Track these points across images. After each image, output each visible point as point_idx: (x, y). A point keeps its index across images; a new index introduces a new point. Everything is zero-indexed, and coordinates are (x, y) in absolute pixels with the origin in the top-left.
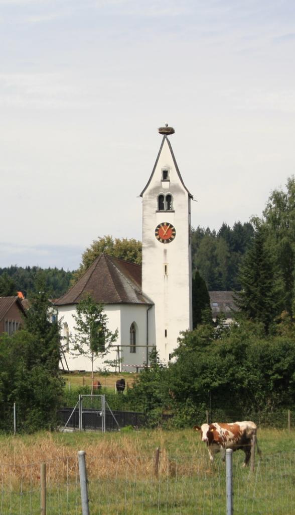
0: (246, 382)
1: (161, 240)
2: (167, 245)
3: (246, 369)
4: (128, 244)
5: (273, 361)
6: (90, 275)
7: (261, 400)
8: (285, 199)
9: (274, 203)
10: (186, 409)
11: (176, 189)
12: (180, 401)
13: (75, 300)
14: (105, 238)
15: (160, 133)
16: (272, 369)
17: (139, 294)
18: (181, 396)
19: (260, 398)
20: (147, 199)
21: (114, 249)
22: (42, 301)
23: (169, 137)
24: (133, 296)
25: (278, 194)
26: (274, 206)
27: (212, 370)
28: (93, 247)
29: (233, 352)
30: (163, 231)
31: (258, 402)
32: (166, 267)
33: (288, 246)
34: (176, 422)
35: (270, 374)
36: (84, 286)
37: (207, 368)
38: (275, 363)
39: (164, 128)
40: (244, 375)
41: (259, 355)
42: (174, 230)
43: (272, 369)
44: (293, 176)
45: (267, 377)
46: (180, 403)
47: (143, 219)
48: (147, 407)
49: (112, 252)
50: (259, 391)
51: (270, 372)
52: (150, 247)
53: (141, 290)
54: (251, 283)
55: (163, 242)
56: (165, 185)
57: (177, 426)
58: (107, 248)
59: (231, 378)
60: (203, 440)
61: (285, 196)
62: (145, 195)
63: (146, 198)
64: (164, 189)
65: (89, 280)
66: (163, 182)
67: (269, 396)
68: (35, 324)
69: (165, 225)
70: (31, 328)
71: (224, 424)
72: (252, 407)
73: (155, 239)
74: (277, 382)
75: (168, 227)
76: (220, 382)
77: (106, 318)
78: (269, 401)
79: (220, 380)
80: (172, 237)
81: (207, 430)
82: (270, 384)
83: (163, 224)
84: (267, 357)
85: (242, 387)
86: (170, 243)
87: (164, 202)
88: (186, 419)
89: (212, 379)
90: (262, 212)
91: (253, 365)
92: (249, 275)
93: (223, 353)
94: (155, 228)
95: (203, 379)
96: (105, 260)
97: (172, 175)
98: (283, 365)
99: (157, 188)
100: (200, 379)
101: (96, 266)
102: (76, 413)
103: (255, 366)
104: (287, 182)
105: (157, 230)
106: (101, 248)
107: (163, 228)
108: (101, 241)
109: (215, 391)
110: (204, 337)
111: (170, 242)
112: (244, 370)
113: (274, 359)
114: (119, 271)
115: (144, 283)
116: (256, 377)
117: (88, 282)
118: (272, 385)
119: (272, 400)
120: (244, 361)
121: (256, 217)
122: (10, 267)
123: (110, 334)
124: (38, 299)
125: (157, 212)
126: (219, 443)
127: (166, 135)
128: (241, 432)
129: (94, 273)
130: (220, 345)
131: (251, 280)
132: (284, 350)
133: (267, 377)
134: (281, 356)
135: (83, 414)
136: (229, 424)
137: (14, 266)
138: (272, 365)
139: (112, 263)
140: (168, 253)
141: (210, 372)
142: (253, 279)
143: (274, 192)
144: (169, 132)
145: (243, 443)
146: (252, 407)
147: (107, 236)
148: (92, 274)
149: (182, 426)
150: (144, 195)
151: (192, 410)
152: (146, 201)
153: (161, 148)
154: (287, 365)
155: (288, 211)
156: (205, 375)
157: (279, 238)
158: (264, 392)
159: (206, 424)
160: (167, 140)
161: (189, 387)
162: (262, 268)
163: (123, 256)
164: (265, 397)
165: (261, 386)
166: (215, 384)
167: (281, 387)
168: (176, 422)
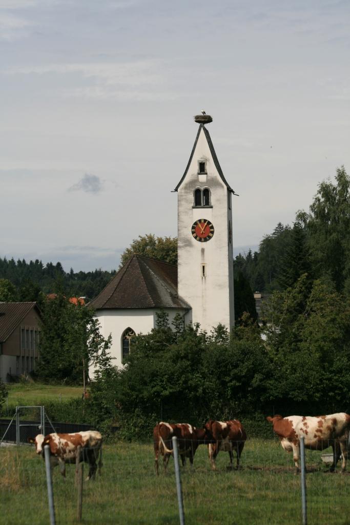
0: (200, 390)
1: (198, 238)
2: (204, 243)
3: (201, 376)
4: (170, 244)
5: (230, 367)
6: (120, 277)
7: (218, 410)
8: (335, 192)
9: (322, 197)
10: (134, 420)
11: (213, 182)
12: (128, 412)
13: (104, 305)
14: (146, 237)
15: (196, 121)
16: (229, 375)
17: (175, 297)
18: (128, 407)
19: (217, 407)
20: (183, 194)
21: (155, 249)
22: (61, 306)
23: (207, 126)
24: (167, 300)
25: (327, 187)
26: (322, 200)
27: (162, 377)
28: (134, 247)
29: (189, 358)
30: (199, 228)
31: (215, 411)
32: (204, 267)
33: (338, 243)
34: (123, 435)
35: (227, 380)
36: (114, 289)
37: (157, 376)
38: (232, 369)
39: (200, 116)
40: (199, 382)
41: (215, 360)
42: (212, 227)
43: (229, 375)
44: (343, 167)
45: (224, 384)
46: (128, 414)
47: (178, 216)
48: (98, 419)
49: (153, 252)
50: (216, 399)
51: (227, 379)
52: (186, 246)
53: (177, 294)
54: (290, 283)
55: (200, 240)
56: (203, 178)
57: (125, 438)
58: (148, 247)
59: (184, 385)
60: (38, 452)
61: (334, 189)
62: (181, 189)
63: (182, 193)
64: (200, 183)
65: (120, 282)
66: (199, 176)
67: (226, 405)
68: (53, 331)
69: (203, 222)
70: (48, 336)
71: (64, 434)
72: (208, 417)
73: (191, 237)
74: (234, 389)
75: (206, 224)
76: (171, 390)
77: (98, 322)
78: (227, 411)
79: (171, 388)
80: (210, 235)
81: (42, 440)
82: (228, 391)
83: (200, 221)
84: (224, 362)
85: (196, 396)
86: (208, 242)
87: (202, 198)
88: (134, 431)
89: (162, 387)
90: (309, 206)
91: (208, 371)
92: (288, 275)
93: (177, 358)
94: (192, 224)
95: (153, 387)
96: (137, 261)
97: (211, 168)
98: (241, 371)
99: (194, 182)
100: (149, 388)
101: (128, 268)
102: (13, 426)
103: (211, 372)
104: (336, 174)
105: (193, 228)
106: (141, 248)
107: (200, 225)
108: (142, 240)
109: (166, 400)
110: (158, 342)
111: (208, 240)
112: (198, 377)
113: (231, 364)
114: (152, 273)
115: (180, 286)
116: (212, 384)
117: (118, 285)
118: (229, 392)
119: (229, 410)
120: (200, 366)
121: (303, 212)
122: (94, 272)
123: (103, 340)
124: (56, 304)
125: (193, 208)
126: (56, 455)
127: (202, 124)
128: (83, 442)
129: (125, 275)
130: (173, 350)
131: (290, 280)
132: (243, 354)
133: (224, 384)
134: (240, 361)
135: (20, 427)
136: (70, 434)
137: (98, 270)
138: (230, 371)
139: (145, 264)
140: (205, 252)
141: (161, 379)
142: (292, 279)
143: (322, 184)
144: (206, 120)
145: (89, 454)
146: (208, 417)
147: (148, 235)
148: (123, 277)
149: (130, 439)
150: (179, 190)
151: (141, 421)
152: (182, 196)
153: (197, 138)
154: (245, 371)
155: (338, 204)
156: (155, 383)
157: (328, 234)
158: (221, 400)
159: (41, 435)
160: (207, 133)
161: (137, 396)
162: (302, 267)
163: (166, 257)
164: (222, 406)
165: (218, 394)
166: (166, 393)
167: (240, 395)
168: (123, 435)
